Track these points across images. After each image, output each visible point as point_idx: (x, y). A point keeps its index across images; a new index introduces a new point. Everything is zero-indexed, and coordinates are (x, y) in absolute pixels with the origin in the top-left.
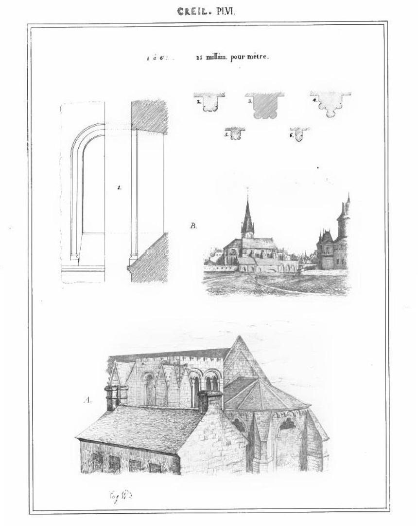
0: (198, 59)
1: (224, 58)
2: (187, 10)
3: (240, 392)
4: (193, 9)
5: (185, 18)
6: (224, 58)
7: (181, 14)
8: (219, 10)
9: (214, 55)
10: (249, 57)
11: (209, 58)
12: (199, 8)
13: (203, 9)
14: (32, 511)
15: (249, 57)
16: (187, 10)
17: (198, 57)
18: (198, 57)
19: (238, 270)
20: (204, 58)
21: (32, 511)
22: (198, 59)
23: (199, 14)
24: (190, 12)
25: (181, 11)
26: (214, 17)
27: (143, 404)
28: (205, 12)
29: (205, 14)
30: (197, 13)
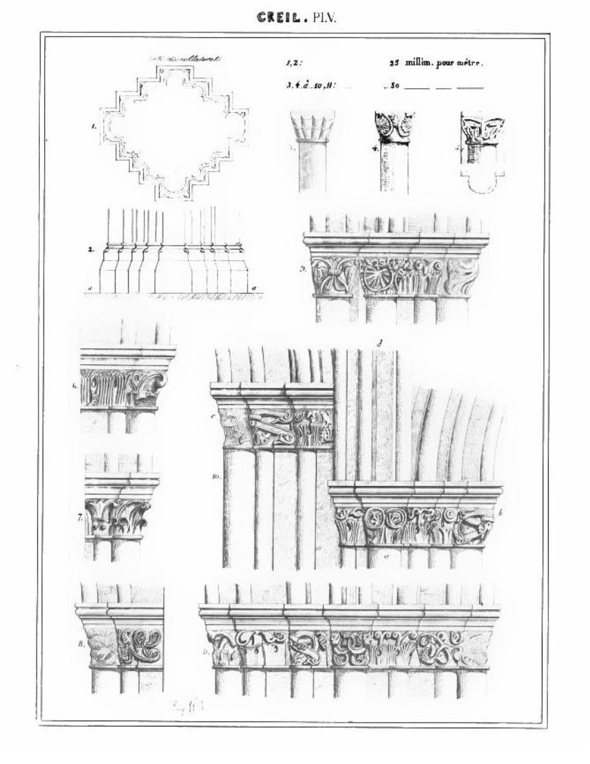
0: (392, 65)
1: (427, 63)
2: (279, 15)
3: (323, 281)
4: (279, 15)
5: (274, 26)
6: (427, 63)
7: (261, 20)
8: (317, 15)
9: (415, 60)
10: (459, 63)
11: (408, 63)
12: (288, 14)
13: (295, 15)
14: (45, 36)
15: (459, 63)
16: (271, 16)
17: (392, 62)
18: (392, 62)
19: (403, 267)
20: (455, 64)
21: (45, 36)
22: (392, 65)
23: (288, 21)
24: (275, 17)
25: (263, 17)
26: (312, 27)
27: (406, 477)
28: (297, 18)
29: (298, 21)
30: (285, 20)
